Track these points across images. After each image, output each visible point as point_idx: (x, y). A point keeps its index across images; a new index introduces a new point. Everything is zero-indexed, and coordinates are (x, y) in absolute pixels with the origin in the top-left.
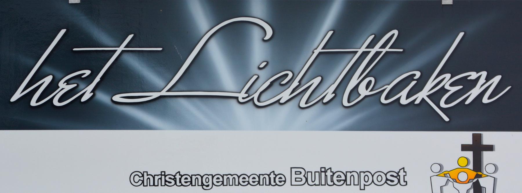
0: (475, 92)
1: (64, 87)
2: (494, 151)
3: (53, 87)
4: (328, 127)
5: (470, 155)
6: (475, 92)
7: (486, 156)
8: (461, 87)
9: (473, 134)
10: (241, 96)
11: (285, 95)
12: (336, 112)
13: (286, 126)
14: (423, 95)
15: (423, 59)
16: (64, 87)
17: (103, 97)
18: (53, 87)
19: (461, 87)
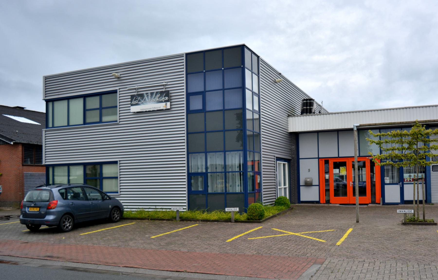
0: (166, 99)
1: (135, 102)
2: (43, 77)
3: (134, 102)
4: (155, 103)
5: (409, 177)
6: (166, 99)
7: (411, 177)
8: (40, 124)
9: (237, 114)
10: (148, 101)
11: (151, 101)
12: (155, 102)
13: (152, 104)
14: (162, 100)
15: (162, 96)
16: (135, 102)
17: (138, 103)
18: (134, 102)
19: (40, 124)
